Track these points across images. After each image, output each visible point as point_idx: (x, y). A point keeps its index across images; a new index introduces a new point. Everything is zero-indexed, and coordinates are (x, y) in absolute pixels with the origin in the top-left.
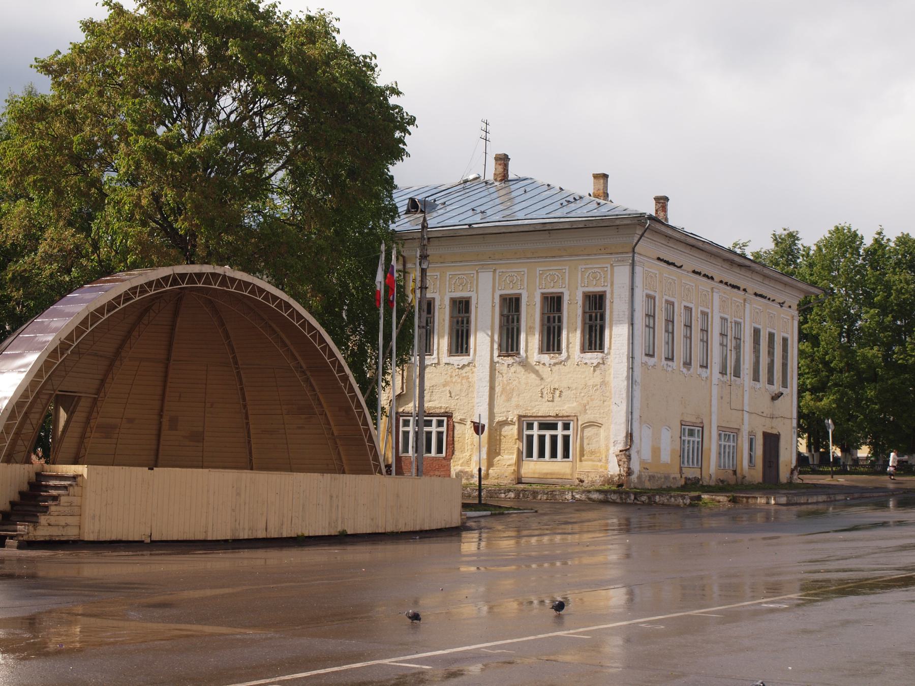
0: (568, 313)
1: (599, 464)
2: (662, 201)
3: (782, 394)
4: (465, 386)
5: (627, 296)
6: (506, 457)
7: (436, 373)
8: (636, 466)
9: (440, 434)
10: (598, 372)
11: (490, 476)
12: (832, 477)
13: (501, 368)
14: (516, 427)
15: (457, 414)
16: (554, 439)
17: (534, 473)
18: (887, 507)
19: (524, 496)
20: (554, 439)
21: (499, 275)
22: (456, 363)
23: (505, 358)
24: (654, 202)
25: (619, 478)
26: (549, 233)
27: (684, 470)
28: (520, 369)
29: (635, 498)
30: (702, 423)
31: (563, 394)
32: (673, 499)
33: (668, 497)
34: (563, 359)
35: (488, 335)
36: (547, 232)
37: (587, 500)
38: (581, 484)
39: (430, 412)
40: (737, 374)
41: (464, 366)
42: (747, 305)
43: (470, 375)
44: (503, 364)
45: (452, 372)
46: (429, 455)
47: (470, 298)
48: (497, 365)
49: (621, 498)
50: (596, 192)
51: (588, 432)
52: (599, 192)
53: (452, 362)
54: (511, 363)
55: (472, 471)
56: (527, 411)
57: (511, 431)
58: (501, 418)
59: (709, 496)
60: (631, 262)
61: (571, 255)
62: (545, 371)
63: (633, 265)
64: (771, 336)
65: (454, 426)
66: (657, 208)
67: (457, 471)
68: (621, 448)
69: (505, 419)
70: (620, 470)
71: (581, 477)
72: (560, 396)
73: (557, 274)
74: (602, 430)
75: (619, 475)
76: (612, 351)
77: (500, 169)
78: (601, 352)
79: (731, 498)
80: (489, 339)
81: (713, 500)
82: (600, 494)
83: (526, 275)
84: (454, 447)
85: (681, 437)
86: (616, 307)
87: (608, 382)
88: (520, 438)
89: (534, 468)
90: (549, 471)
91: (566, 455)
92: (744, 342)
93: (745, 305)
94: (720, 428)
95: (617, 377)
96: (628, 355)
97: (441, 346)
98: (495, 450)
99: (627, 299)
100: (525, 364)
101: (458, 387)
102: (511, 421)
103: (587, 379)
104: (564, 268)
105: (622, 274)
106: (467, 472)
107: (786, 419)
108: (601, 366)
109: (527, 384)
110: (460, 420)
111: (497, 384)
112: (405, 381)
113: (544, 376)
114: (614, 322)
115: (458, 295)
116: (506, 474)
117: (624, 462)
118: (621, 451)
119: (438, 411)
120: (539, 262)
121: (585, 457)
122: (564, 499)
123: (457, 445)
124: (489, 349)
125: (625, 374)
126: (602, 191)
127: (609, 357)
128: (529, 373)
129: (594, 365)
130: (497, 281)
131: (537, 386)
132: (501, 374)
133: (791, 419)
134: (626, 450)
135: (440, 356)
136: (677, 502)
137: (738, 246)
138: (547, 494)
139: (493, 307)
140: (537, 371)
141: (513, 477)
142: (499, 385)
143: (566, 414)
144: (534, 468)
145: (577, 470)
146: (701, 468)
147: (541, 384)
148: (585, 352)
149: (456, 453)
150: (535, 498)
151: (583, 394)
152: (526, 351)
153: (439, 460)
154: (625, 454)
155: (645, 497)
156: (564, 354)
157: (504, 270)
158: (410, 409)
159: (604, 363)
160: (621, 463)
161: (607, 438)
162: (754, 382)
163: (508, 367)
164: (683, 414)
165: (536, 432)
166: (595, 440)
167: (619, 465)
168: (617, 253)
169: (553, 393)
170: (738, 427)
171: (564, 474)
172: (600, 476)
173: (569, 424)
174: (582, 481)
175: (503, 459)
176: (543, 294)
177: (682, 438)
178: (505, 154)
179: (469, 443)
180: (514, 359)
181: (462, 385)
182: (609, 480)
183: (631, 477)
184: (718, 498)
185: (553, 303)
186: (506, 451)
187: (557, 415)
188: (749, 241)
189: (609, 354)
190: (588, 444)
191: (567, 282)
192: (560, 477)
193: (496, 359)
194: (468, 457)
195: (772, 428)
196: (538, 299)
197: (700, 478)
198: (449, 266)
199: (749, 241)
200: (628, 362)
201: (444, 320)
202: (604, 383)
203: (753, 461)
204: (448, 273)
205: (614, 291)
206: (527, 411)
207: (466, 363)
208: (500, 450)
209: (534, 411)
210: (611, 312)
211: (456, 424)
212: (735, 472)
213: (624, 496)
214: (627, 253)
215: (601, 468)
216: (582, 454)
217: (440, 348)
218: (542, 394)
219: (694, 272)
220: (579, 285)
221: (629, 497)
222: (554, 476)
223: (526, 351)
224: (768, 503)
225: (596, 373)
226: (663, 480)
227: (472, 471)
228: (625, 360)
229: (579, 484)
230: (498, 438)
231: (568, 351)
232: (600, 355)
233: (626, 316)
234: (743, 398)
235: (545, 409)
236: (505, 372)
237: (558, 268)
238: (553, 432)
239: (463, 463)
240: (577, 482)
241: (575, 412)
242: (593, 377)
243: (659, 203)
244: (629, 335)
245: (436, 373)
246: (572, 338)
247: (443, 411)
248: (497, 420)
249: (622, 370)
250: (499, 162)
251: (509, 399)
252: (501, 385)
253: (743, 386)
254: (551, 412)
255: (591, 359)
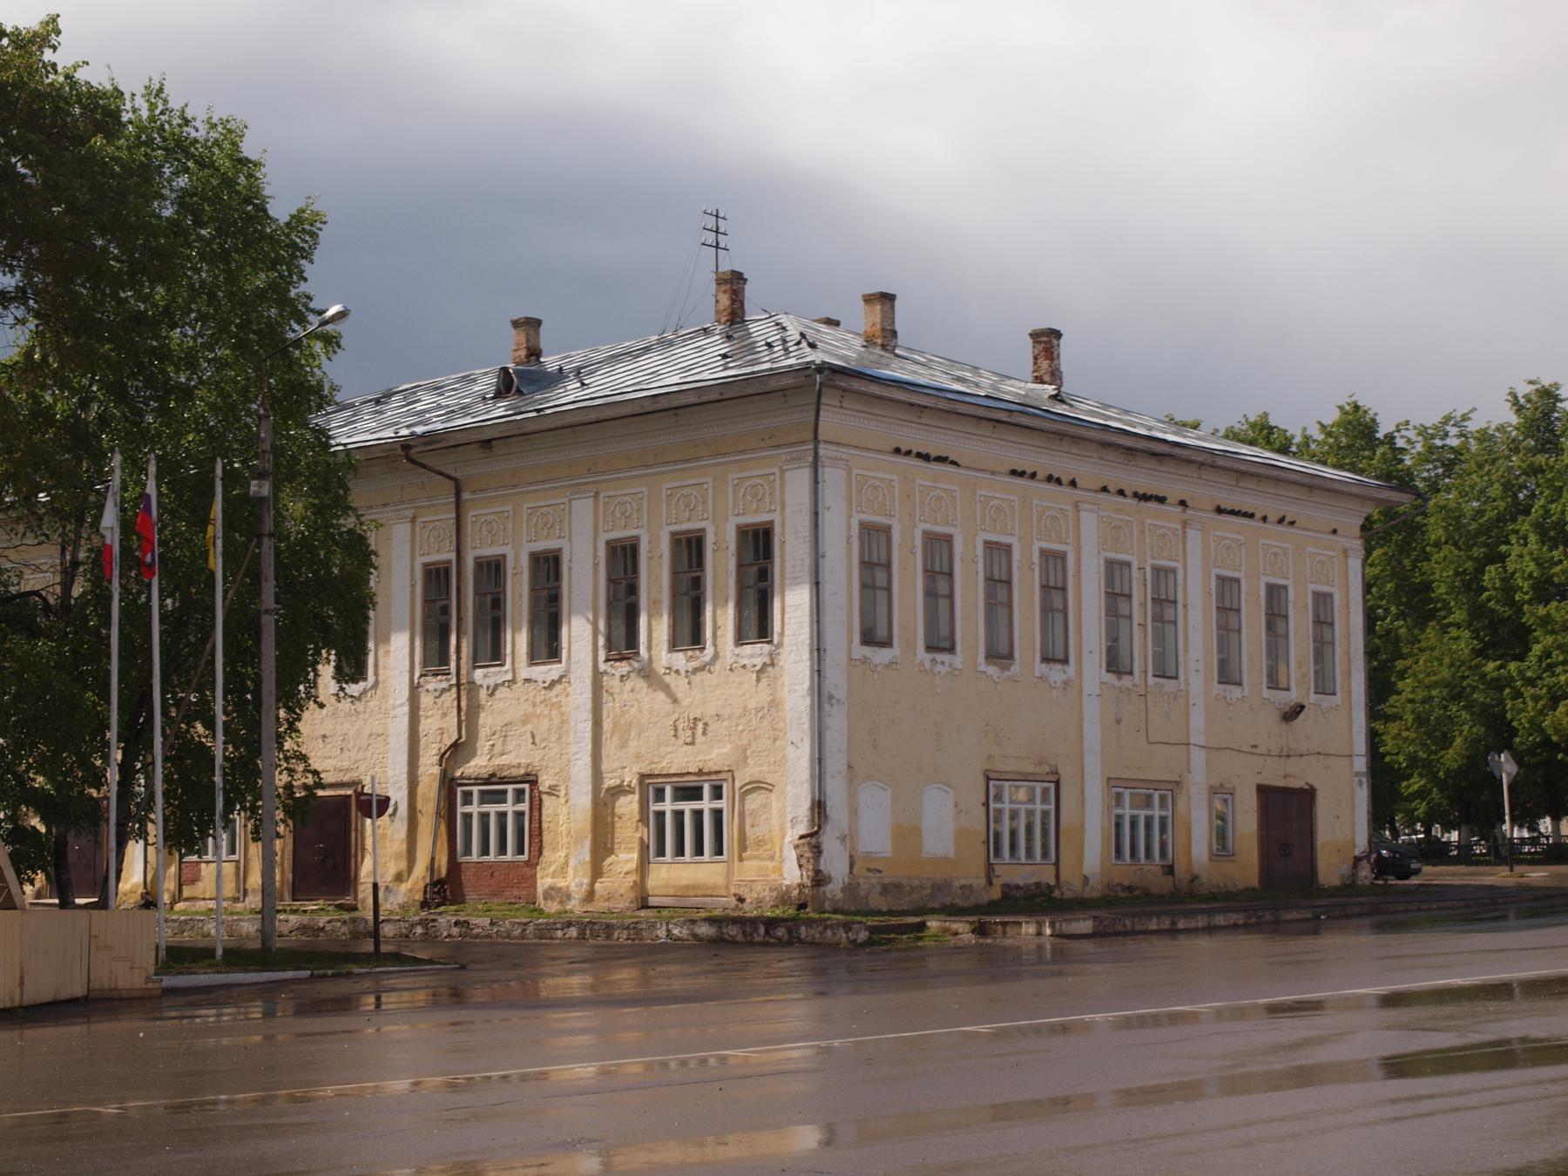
0: (714, 567)
1: (770, 864)
2: (1044, 339)
3: (1302, 707)
4: (556, 722)
5: (807, 528)
6: (622, 856)
7: (511, 699)
8: (836, 865)
9: (520, 815)
10: (764, 682)
11: (597, 895)
12: (1511, 870)
13: (611, 683)
14: (636, 797)
15: (544, 777)
16: (698, 815)
17: (667, 886)
18: (224, 950)
19: (592, 934)
20: (698, 815)
21: (605, 504)
22: (540, 679)
23: (617, 664)
24: (1029, 341)
25: (800, 890)
26: (676, 415)
27: (998, 870)
28: (640, 684)
29: (767, 932)
30: (1057, 773)
31: (710, 729)
32: (829, 933)
33: (821, 928)
34: (707, 659)
35: (588, 620)
36: (672, 412)
37: (690, 938)
38: (740, 905)
39: (504, 774)
40: (1165, 669)
41: (553, 684)
42: (1191, 532)
43: (564, 700)
44: (613, 675)
45: (535, 697)
46: (502, 858)
47: (560, 550)
48: (605, 678)
49: (744, 933)
50: (869, 330)
51: (753, 801)
52: (874, 329)
53: (534, 677)
54: (625, 673)
55: (568, 887)
56: (653, 766)
57: (628, 806)
58: (612, 781)
59: (939, 923)
60: (811, 459)
61: (715, 456)
62: (678, 684)
63: (815, 466)
64: (1275, 594)
65: (541, 800)
66: (1036, 352)
67: (546, 887)
68: (803, 831)
69: (618, 782)
70: (802, 875)
71: (740, 892)
72: (704, 734)
73: (695, 493)
74: (773, 796)
75: (799, 885)
76: (786, 640)
77: (725, 300)
78: (768, 642)
79: (977, 925)
80: (589, 628)
81: (945, 930)
82: (710, 925)
83: (645, 500)
84: (541, 841)
85: (987, 804)
86: (791, 551)
87: (781, 700)
88: (644, 819)
89: (670, 876)
90: (690, 882)
91: (719, 850)
92: (1185, 606)
93: (1184, 533)
94: (1113, 783)
95: (796, 690)
96: (811, 644)
97: (517, 648)
98: (605, 844)
99: (808, 534)
100: (647, 674)
101: (545, 724)
102: (629, 786)
103: (747, 696)
104: (704, 480)
105: (798, 482)
106: (561, 888)
107: (1331, 758)
108: (770, 669)
109: (651, 712)
110: (549, 787)
111: (605, 716)
112: (463, 718)
113: (679, 695)
114: (787, 581)
115: (541, 546)
116: (622, 891)
117: (808, 858)
118: (802, 837)
119: (515, 772)
120: (665, 472)
121: (749, 852)
122: (654, 937)
123: (546, 837)
124: (590, 648)
125: (807, 684)
126: (879, 327)
127: (781, 651)
128: (655, 691)
129: (758, 668)
130: (601, 515)
131: (668, 715)
132: (612, 694)
133: (1351, 756)
134: (811, 835)
135: (517, 666)
136: (835, 939)
137: (1452, 422)
138: (628, 928)
139: (596, 565)
140: (668, 686)
141: (632, 895)
142: (608, 717)
143: (715, 768)
144: (670, 876)
145: (735, 879)
146: (1057, 864)
147: (674, 712)
148: (742, 644)
149: (546, 852)
150: (609, 937)
151: (740, 728)
152: (649, 648)
153: (518, 866)
154: (809, 844)
155: (783, 930)
156: (709, 650)
157: (612, 493)
158: (472, 770)
159: (773, 665)
160: (803, 861)
161: (782, 814)
162: (1222, 686)
163: (622, 681)
164: (990, 757)
165: (668, 806)
166: (762, 818)
167: (800, 866)
168: (789, 445)
169: (693, 729)
170: (1177, 779)
171: (715, 887)
172: (770, 889)
173: (720, 787)
174: (741, 900)
175: (618, 862)
176: (673, 534)
177: (992, 805)
178: (733, 272)
179: (564, 833)
180: (630, 665)
181: (551, 719)
182: (783, 896)
183: (822, 889)
184: (955, 926)
185: (690, 548)
186: (623, 846)
187: (700, 770)
188: (1474, 409)
189: (780, 645)
190: (753, 826)
191: (710, 508)
192: (709, 892)
193: (602, 667)
194: (562, 860)
195: (1285, 777)
196: (665, 545)
197: (1053, 883)
198: (527, 492)
199: (1474, 409)
200: (812, 659)
201: (521, 596)
202: (775, 704)
203: (1230, 843)
204: (526, 506)
205: (787, 520)
206: (653, 766)
207: (556, 678)
208: (613, 843)
209: (664, 764)
210: (783, 561)
211: (544, 797)
212: (1169, 870)
213: (748, 929)
214: (804, 442)
215: (773, 872)
216: (743, 847)
217: (516, 651)
218: (676, 730)
219: (1014, 473)
220: (730, 513)
221: (757, 929)
222: (699, 892)
223: (649, 648)
224: (1039, 934)
225: (760, 684)
226: (928, 891)
227: (568, 887)
228: (806, 656)
229: (737, 906)
230: (609, 819)
231: (715, 645)
232: (767, 648)
233: (807, 568)
234: (1188, 719)
235: (680, 759)
236: (616, 690)
237: (694, 482)
238: (695, 805)
239: (555, 871)
240: (734, 901)
241: (727, 763)
242: (757, 692)
243: (1039, 342)
244: (811, 607)
245: (511, 699)
246: (721, 618)
247: (522, 771)
248: (605, 786)
249: (801, 675)
250: (724, 287)
251: (623, 745)
252: (611, 717)
253: (1187, 696)
254: (690, 765)
255: (752, 656)
